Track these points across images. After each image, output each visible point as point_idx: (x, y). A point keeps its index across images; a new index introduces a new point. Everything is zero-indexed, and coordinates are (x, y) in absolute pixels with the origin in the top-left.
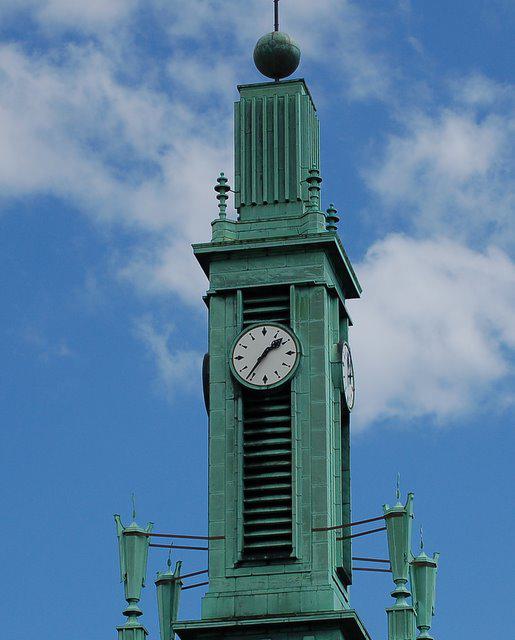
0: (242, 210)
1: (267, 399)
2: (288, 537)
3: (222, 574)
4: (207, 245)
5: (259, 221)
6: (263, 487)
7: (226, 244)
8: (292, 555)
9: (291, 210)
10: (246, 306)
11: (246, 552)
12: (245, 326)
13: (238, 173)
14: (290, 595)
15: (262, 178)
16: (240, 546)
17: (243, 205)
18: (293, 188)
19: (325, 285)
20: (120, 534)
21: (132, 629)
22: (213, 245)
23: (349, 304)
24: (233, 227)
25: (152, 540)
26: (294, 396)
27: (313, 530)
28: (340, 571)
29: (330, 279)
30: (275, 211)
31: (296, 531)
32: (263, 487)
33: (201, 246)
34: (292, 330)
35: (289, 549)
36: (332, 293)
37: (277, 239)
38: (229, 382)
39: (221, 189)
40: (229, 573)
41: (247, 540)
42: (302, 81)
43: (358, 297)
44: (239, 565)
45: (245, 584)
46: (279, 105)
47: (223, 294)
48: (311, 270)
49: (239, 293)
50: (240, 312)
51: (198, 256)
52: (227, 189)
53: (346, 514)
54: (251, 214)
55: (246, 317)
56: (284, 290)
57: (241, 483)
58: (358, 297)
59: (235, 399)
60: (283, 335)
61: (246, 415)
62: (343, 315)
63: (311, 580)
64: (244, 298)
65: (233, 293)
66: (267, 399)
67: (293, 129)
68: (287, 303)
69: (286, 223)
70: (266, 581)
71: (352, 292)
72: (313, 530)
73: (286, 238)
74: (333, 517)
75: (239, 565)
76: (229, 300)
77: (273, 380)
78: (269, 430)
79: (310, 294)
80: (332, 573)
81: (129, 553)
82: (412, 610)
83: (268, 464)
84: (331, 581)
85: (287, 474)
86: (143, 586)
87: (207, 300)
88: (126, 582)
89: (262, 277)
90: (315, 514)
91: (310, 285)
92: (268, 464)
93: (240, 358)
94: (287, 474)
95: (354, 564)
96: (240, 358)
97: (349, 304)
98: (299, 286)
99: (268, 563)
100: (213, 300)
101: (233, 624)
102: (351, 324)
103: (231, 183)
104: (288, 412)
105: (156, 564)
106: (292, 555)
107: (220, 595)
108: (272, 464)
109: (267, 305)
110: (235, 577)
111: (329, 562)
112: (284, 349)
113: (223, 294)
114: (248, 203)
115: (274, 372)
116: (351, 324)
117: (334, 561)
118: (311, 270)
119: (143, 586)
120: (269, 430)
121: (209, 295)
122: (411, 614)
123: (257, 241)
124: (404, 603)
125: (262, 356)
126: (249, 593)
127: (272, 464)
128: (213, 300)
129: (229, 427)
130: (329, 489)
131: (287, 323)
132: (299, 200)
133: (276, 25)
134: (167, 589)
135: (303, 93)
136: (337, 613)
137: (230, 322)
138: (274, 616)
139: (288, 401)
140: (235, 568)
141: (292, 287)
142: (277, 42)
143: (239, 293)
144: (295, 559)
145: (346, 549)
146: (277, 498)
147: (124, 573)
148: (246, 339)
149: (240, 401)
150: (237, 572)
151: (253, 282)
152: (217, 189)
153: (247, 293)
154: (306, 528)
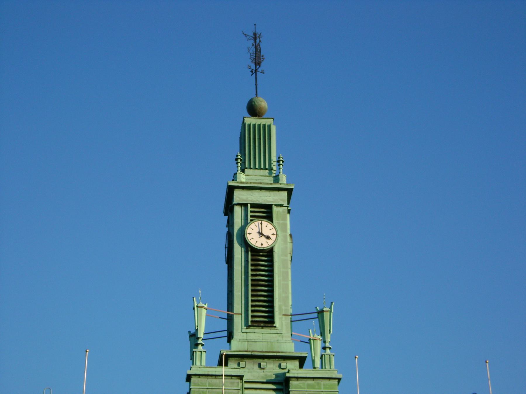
7: (241, 183)
8: (274, 325)
45: (252, 336)
56: (269, 207)
63: (282, 337)
64: (251, 207)
66: (261, 254)
90: (283, 308)
98: (277, 205)
99: (263, 327)
106: (274, 325)
141: (273, 206)
144: (275, 327)
149: (250, 253)
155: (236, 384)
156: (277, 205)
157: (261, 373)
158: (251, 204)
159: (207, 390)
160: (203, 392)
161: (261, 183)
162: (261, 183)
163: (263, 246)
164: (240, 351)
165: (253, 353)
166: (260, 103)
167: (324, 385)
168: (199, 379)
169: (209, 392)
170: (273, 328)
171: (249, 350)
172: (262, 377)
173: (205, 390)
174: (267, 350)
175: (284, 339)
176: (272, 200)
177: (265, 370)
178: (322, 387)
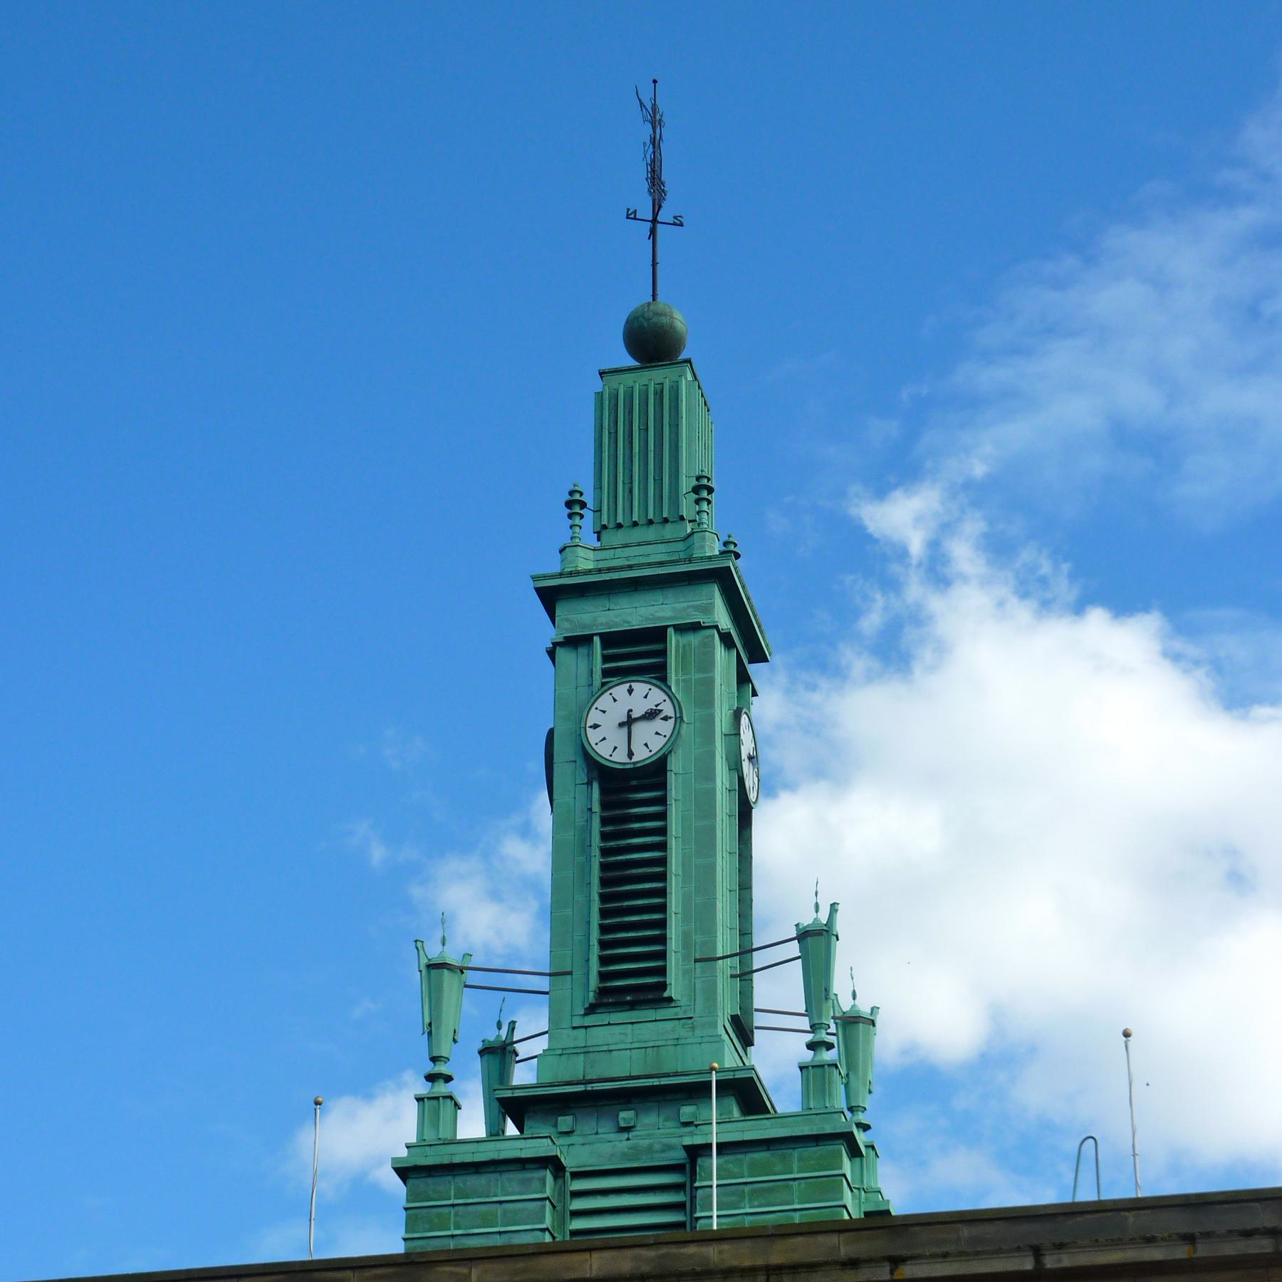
0: (604, 535)
1: (634, 783)
2: (662, 971)
3: (566, 1024)
4: (552, 577)
5: (626, 546)
6: (627, 919)
7: (578, 573)
8: (666, 994)
9: (669, 531)
10: (606, 659)
11: (602, 992)
12: (603, 684)
13: (598, 487)
14: (663, 1050)
15: (631, 491)
16: (594, 982)
17: (604, 527)
18: (675, 502)
19: (716, 627)
20: (423, 968)
21: (437, 1098)
22: (561, 575)
23: (752, 669)
24: (591, 554)
25: (471, 977)
26: (672, 780)
27: (696, 961)
28: (735, 1021)
29: (724, 620)
30: (651, 533)
31: (674, 963)
32: (627, 919)
33: (545, 577)
34: (670, 688)
35: (664, 986)
36: (726, 639)
37: (650, 565)
38: (580, 761)
39: (574, 504)
40: (577, 1022)
41: (603, 976)
42: (689, 361)
43: (767, 660)
44: (591, 1009)
45: (600, 1036)
46: (655, 393)
47: (576, 642)
48: (697, 608)
49: (597, 639)
50: (598, 665)
51: (538, 590)
52: (583, 505)
53: (745, 932)
54: (612, 538)
55: (606, 673)
56: (657, 635)
57: (596, 898)
58: (767, 660)
59: (589, 783)
60: (657, 696)
61: (604, 806)
62: (743, 678)
63: (693, 1028)
64: (604, 647)
65: (585, 640)
66: (634, 783)
67: (675, 426)
68: (664, 653)
69: (662, 548)
70: (629, 1031)
71: (758, 655)
72: (696, 961)
73: (661, 564)
74: (725, 942)
75: (591, 1009)
76: (583, 650)
77: (641, 755)
78: (636, 825)
79: (694, 639)
80: (723, 1021)
81: (434, 997)
82: (836, 1067)
83: (634, 871)
84: (721, 1031)
85: (660, 963)
86: (455, 1041)
87: (551, 653)
88: (430, 1034)
89: (629, 619)
90: (698, 938)
91: (695, 627)
92: (634, 871)
93: (595, 726)
94: (660, 963)
95: (759, 1019)
96: (595, 726)
97: (752, 669)
98: (681, 629)
99: (632, 1006)
100: (560, 652)
101: (580, 1088)
102: (755, 694)
103: (588, 498)
104: (663, 801)
105: (472, 1018)
106: (666, 994)
107: (564, 1053)
108: (640, 871)
109: (637, 654)
110: (586, 1027)
111: (719, 1006)
112: (658, 724)
113: (576, 642)
114: (611, 526)
115: (648, 742)
116: (755, 694)
117: (727, 1006)
118: (697, 608)
119: (455, 1041)
120: (636, 825)
121: (555, 644)
122: (835, 1072)
123: (621, 568)
124: (828, 1056)
125: (623, 724)
126: (605, 1048)
127: (640, 871)
128: (560, 652)
129: (580, 821)
130: (719, 905)
131: (664, 679)
132: (682, 518)
133: (654, 296)
134: (494, 1060)
135: (690, 377)
136: (729, 1070)
137: (583, 680)
138: (638, 1077)
139: (663, 786)
140: (586, 1014)
141: (670, 631)
142: (656, 314)
143: (597, 639)
144: (670, 999)
145: (746, 995)
146: (646, 917)
147: (427, 1021)
148: (604, 701)
149: (596, 786)
150: (589, 1020)
151: (617, 625)
152: (569, 504)
153: (610, 639)
154: (686, 958)
155: (536, 1184)
156: (681, 629)
157: (621, 1143)
158: (600, 635)
159: (453, 1210)
160: (439, 1215)
161: (630, 567)
162: (630, 567)
163: (635, 759)
164: (551, 1085)
165: (589, 1088)
166: (655, 320)
167: (800, 1159)
168: (430, 1180)
169: (456, 1215)
170: (665, 1005)
171: (588, 1077)
172: (624, 1156)
173: (445, 1210)
174: (567, 1079)
175: (698, 1032)
176: (669, 614)
177: (631, 1135)
178: (795, 1166)
